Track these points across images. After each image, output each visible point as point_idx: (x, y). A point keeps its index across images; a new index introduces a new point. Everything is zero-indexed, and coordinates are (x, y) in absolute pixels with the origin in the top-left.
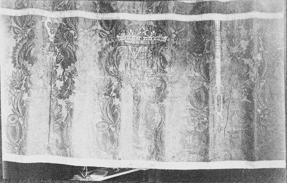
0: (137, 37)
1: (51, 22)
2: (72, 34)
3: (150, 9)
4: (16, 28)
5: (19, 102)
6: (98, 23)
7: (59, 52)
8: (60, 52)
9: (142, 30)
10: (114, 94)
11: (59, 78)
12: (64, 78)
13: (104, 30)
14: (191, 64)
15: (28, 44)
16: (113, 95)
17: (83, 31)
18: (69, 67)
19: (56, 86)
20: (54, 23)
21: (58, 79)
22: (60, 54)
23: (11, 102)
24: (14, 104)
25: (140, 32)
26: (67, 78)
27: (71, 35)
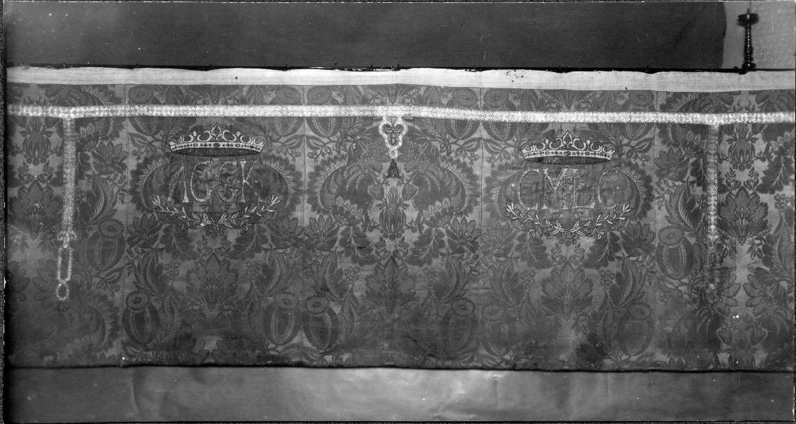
0: (559, 151)
1: (390, 124)
2: (437, 149)
3: (583, 102)
4: (314, 138)
5: (148, 268)
6: (481, 127)
7: (409, 178)
8: (411, 179)
9: (568, 139)
10: (517, 254)
11: (409, 225)
12: (421, 228)
13: (493, 139)
14: (661, 199)
15: (350, 169)
16: (514, 256)
17: (455, 143)
18: (430, 206)
19: (406, 241)
20: (395, 125)
21: (409, 228)
22: (411, 183)
23: (133, 269)
24: (138, 273)
25: (565, 142)
26: (426, 227)
27: (433, 149)
